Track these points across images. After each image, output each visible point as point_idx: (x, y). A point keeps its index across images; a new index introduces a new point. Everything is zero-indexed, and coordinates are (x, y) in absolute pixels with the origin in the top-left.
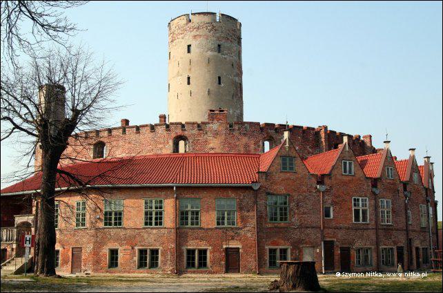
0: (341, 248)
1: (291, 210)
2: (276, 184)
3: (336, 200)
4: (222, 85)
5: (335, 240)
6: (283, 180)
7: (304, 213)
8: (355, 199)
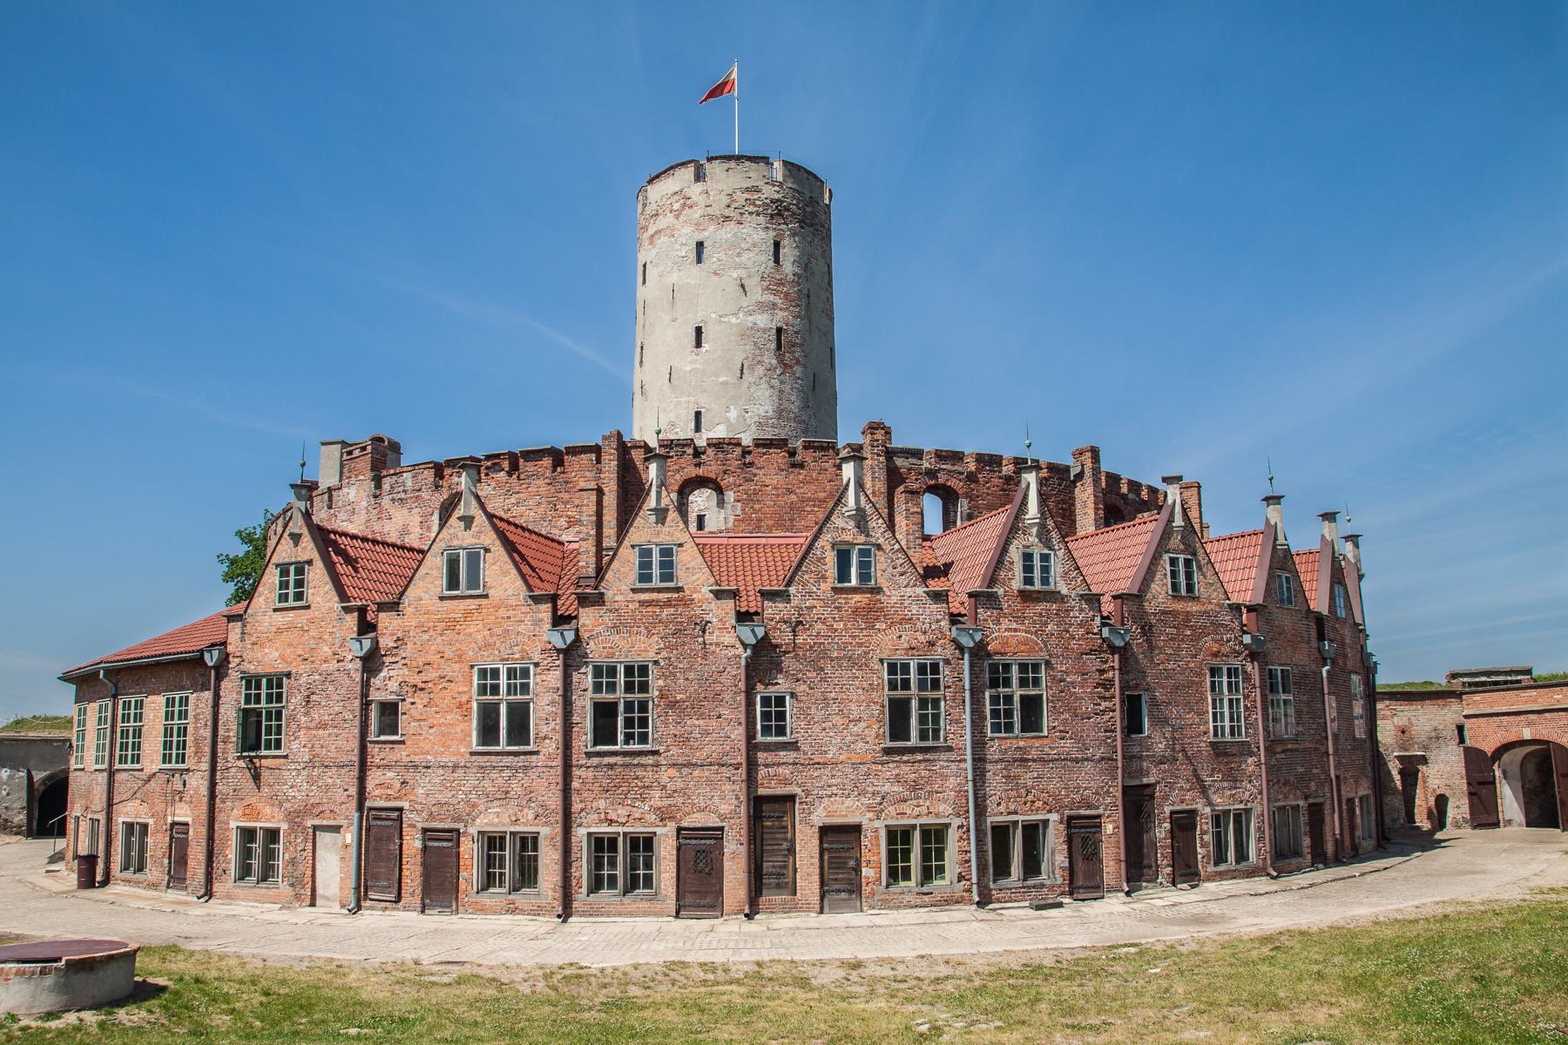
0: (425, 830)
1: (292, 718)
2: (262, 646)
3: (417, 679)
4: (706, 346)
5: (406, 805)
6: (279, 631)
7: (323, 726)
8: (483, 673)
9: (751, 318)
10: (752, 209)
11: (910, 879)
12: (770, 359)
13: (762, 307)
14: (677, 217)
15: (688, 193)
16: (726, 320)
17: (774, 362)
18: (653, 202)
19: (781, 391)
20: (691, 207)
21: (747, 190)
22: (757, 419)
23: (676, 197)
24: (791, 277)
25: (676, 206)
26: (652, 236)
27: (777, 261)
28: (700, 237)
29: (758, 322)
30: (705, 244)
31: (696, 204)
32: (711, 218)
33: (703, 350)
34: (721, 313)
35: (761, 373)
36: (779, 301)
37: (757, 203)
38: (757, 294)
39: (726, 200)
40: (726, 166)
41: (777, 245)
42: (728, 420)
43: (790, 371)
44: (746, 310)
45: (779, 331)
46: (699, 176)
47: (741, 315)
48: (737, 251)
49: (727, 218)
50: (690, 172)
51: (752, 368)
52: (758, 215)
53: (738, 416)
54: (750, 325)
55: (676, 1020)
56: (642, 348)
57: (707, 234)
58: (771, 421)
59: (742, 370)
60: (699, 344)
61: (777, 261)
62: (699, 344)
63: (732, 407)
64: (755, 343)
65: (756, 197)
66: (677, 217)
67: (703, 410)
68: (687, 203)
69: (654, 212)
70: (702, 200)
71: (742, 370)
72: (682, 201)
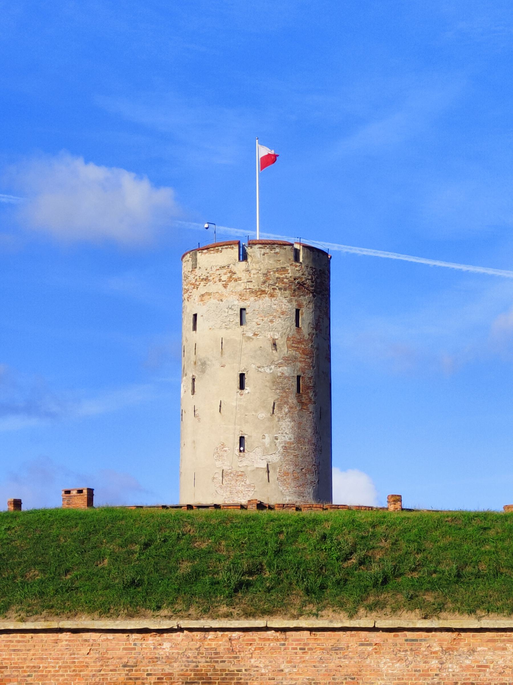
4: (248, 389)
9: (280, 369)
10: (281, 285)
11: (242, 669)
12: (292, 400)
13: (288, 360)
14: (225, 286)
15: (234, 269)
16: (262, 370)
17: (295, 401)
18: (203, 268)
19: (300, 423)
20: (236, 280)
21: (278, 270)
22: (283, 444)
23: (225, 271)
24: (307, 337)
25: (224, 278)
26: (203, 295)
27: (297, 325)
28: (242, 305)
29: (285, 372)
30: (248, 311)
31: (240, 279)
32: (253, 292)
33: (245, 391)
34: (259, 365)
35: (287, 410)
36: (299, 355)
37: (285, 280)
38: (284, 350)
39: (262, 279)
40: (263, 251)
41: (297, 311)
42: (264, 444)
43: (305, 407)
44: (276, 363)
45: (299, 377)
46: (244, 256)
47: (273, 367)
48: (271, 318)
49: (263, 292)
50: (235, 252)
51: (280, 408)
52: (285, 289)
53: (271, 442)
54: (279, 374)
55: (360, 515)
56: (194, 380)
57: (248, 303)
58: (292, 446)
59: (274, 408)
60: (242, 386)
61: (297, 325)
62: (242, 386)
63: (266, 435)
64: (283, 388)
65: (283, 276)
66: (225, 286)
67: (245, 436)
68: (232, 276)
69: (205, 277)
70: (244, 276)
71: (274, 408)
72: (229, 275)
